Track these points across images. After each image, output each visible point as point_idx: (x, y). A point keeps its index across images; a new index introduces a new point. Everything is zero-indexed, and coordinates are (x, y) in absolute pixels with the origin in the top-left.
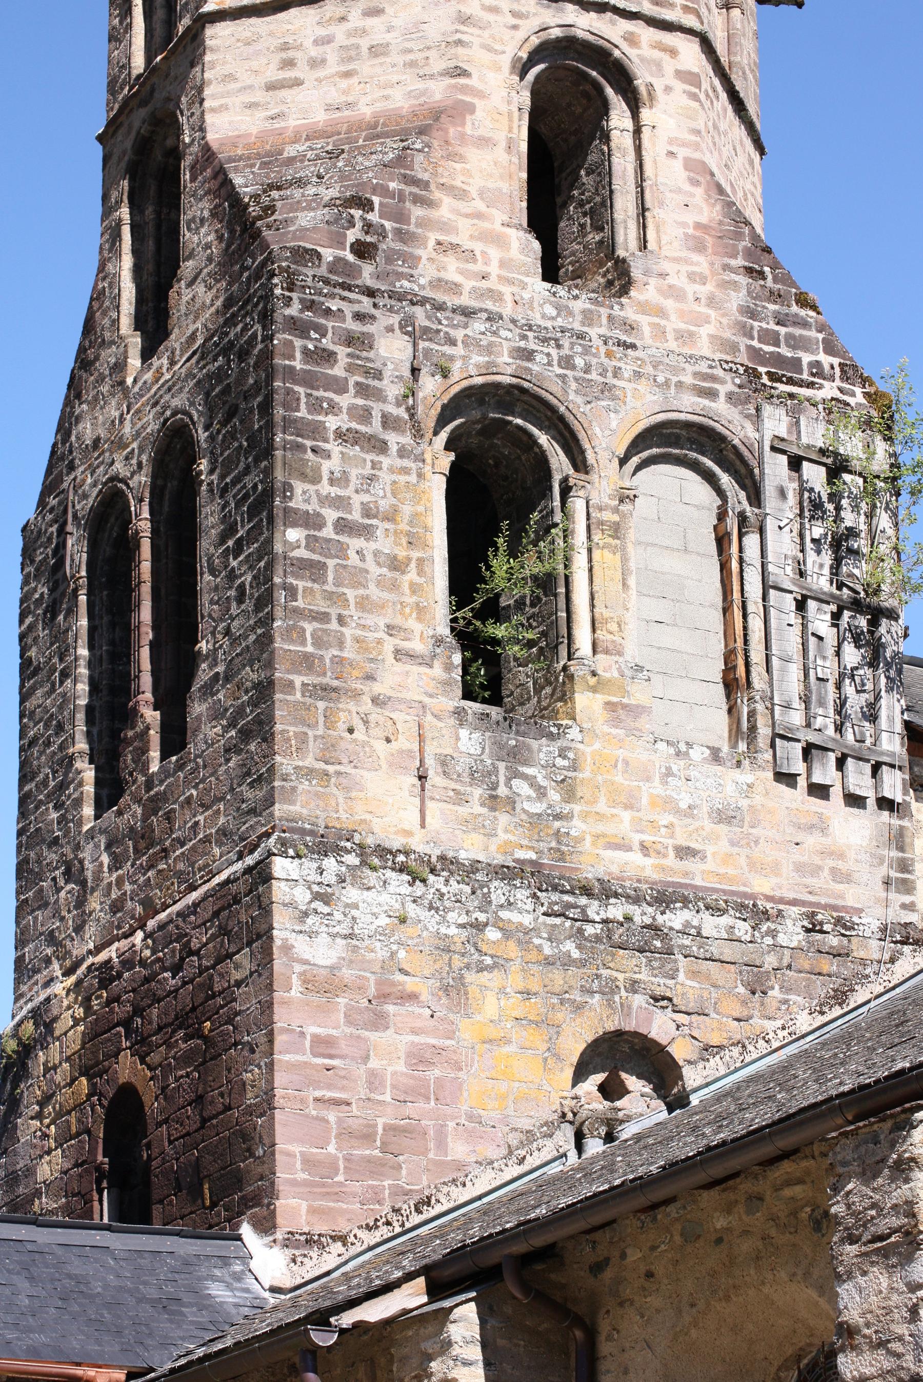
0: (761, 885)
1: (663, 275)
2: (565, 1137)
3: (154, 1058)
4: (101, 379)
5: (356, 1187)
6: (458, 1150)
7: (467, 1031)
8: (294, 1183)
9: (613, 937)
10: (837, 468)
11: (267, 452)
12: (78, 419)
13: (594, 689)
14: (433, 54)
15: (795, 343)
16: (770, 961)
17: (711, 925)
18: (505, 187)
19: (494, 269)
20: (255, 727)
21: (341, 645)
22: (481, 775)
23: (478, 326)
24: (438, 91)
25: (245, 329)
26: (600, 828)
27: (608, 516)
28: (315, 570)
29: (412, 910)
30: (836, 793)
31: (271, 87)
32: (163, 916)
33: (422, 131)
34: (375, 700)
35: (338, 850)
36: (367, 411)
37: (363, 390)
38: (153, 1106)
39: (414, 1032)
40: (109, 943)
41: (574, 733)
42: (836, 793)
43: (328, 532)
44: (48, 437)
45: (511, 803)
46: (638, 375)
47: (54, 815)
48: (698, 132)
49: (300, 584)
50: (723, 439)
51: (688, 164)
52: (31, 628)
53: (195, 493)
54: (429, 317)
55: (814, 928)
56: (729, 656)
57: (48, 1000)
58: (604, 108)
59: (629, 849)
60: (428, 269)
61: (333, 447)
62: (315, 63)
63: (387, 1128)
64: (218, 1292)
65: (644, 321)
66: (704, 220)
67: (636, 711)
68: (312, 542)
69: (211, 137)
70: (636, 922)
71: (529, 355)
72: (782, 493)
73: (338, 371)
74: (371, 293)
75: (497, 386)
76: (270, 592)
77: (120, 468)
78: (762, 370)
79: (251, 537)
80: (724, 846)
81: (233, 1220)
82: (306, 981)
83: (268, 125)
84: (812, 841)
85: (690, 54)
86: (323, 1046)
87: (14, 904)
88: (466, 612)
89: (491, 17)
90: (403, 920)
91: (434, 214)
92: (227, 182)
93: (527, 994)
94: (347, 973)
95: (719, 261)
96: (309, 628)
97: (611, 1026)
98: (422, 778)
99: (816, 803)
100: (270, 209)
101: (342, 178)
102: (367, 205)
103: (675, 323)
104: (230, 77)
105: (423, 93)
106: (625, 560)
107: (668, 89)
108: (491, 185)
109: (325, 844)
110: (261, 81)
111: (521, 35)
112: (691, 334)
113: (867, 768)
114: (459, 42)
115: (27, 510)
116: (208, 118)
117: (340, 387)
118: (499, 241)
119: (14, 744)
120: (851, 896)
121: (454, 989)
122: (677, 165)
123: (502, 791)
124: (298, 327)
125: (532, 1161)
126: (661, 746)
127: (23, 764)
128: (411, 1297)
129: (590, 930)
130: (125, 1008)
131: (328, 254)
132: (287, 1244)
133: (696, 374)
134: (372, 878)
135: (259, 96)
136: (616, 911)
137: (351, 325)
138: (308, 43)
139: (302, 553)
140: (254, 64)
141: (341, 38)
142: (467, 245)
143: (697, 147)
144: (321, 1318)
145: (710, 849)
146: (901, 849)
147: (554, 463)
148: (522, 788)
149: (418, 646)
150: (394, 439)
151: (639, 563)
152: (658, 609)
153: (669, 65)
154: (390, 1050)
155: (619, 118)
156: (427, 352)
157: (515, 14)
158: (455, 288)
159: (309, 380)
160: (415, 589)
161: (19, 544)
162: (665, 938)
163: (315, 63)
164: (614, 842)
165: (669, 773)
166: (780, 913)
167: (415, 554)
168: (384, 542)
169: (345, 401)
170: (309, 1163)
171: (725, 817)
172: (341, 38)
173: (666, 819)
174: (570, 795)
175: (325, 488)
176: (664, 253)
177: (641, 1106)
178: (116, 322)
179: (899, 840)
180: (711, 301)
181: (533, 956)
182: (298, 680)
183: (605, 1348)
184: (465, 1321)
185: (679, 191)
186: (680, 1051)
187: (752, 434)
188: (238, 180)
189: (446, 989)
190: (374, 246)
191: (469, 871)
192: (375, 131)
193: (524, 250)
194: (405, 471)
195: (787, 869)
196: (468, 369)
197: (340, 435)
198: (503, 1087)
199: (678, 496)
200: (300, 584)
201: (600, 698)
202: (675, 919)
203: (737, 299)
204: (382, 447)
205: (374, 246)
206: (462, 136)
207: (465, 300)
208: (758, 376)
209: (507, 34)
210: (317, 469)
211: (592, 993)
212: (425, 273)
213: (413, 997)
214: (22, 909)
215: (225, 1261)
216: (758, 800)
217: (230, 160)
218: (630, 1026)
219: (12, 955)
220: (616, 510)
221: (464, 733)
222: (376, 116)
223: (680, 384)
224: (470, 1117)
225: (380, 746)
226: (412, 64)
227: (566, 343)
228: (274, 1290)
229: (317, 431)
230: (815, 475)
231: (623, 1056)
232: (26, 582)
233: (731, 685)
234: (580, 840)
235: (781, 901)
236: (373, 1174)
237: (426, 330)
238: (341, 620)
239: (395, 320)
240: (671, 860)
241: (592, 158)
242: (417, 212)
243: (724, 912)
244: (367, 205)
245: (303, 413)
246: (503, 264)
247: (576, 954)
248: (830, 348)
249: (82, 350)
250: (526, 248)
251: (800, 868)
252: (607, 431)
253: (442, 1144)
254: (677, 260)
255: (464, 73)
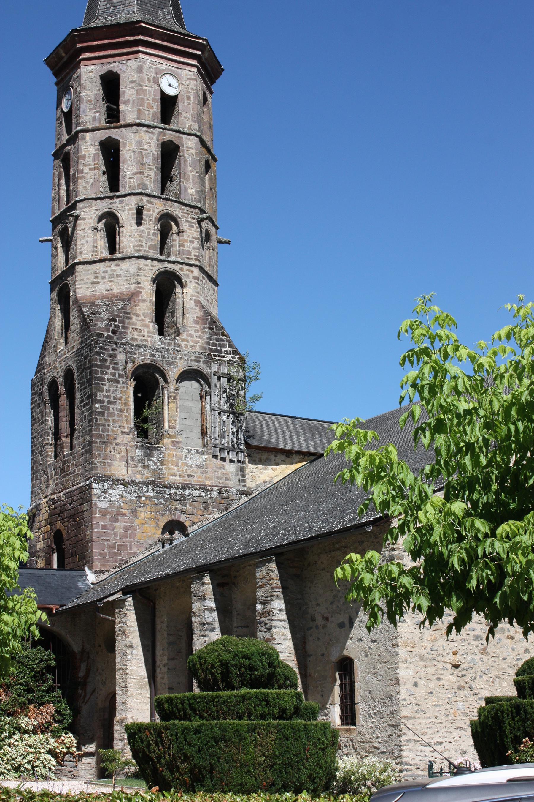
0: (208, 483)
1: (188, 331)
2: (159, 546)
3: (66, 524)
4: (50, 348)
5: (111, 559)
6: (135, 549)
7: (137, 522)
8: (97, 559)
9: (172, 497)
10: (230, 379)
11: (91, 385)
12: (45, 356)
13: (168, 438)
14: (132, 278)
15: (221, 345)
16: (210, 501)
17: (196, 493)
18: (149, 312)
19: (146, 334)
20: (88, 450)
21: (108, 431)
22: (142, 461)
23: (142, 349)
24: (133, 287)
25: (86, 352)
26: (170, 471)
27: (173, 395)
28: (102, 414)
29: (124, 494)
30: (227, 460)
31: (93, 283)
32: (67, 490)
33: (129, 300)
34: (116, 444)
35: (107, 481)
36: (115, 373)
37: (114, 368)
38: (64, 533)
39: (125, 522)
40: (54, 493)
41: (164, 449)
42: (227, 460)
43: (105, 404)
44: (37, 358)
45: (148, 467)
46: (181, 358)
47: (41, 458)
48: (198, 293)
49: (99, 417)
50: (202, 372)
51: (195, 301)
52: (34, 407)
53: (74, 389)
54: (129, 348)
55: (220, 492)
56: (202, 425)
57: (39, 504)
58: (175, 287)
59: (176, 476)
60: (131, 335)
61: (107, 383)
62: (103, 278)
63: (118, 545)
64: (80, 585)
65: (183, 344)
66: (198, 316)
67: (178, 442)
68: (101, 407)
69: (77, 295)
70: (177, 493)
71: (153, 356)
72: (216, 386)
73: (108, 364)
74: (116, 343)
75: (146, 364)
76: (92, 419)
77: (55, 374)
78: (212, 354)
79: (88, 404)
80: (199, 473)
81: (84, 566)
82: (100, 512)
83: (91, 293)
84: (221, 471)
85: (196, 272)
86: (104, 527)
87: (30, 477)
88: (138, 420)
89: (146, 268)
90: (122, 497)
91: (131, 321)
92: (81, 310)
93: (151, 512)
94: (109, 510)
95: (202, 326)
96: (101, 428)
97: (171, 519)
98: (127, 462)
99: (223, 463)
100: (92, 320)
101: (109, 313)
102: (115, 320)
103: (192, 340)
104: (82, 280)
105: (129, 288)
106: (177, 405)
107: (190, 282)
108: (146, 312)
109: (104, 479)
110: (89, 281)
111: (154, 271)
112: (195, 346)
113: (235, 453)
114: (138, 275)
115: (33, 376)
116: (77, 291)
117: (108, 367)
118: (147, 326)
119: (30, 437)
120: (230, 484)
121: (134, 512)
122: (192, 302)
123: (146, 464)
124: (98, 354)
125: (152, 551)
126: (185, 450)
127: (32, 443)
128: (119, 595)
129: (166, 496)
130: (58, 511)
131: (106, 334)
132: (95, 573)
133: (195, 357)
134: (115, 487)
135: (89, 285)
136: (173, 491)
137: (111, 352)
138: (101, 272)
139: (99, 410)
140: (88, 277)
141: (109, 272)
142: (140, 328)
143: (197, 296)
144: (100, 600)
145: (196, 475)
146: (243, 472)
147: (160, 381)
148: (151, 463)
149: (126, 430)
150: (121, 380)
151: (180, 407)
152: (184, 415)
153: (191, 275)
154: (119, 527)
155: (178, 290)
156: (129, 357)
157: (152, 266)
158: (136, 340)
159: (101, 367)
160: (126, 416)
161: (30, 385)
162: (184, 497)
163: (103, 278)
164: (173, 475)
165: (186, 457)
166: (212, 490)
167: (126, 408)
168: (118, 406)
169: (109, 371)
170: (100, 554)
171: (199, 467)
172: (109, 272)
173: (185, 468)
174: (162, 463)
175: (105, 393)
176: (189, 325)
177: (179, 538)
178: (54, 334)
179: (242, 470)
180: (200, 337)
181: (153, 503)
182: (98, 441)
183: (157, 607)
184: (130, 601)
185: (193, 309)
186: (187, 524)
187: (209, 371)
188: (84, 310)
189: (132, 512)
190: (117, 331)
191: (137, 484)
192: (118, 298)
193: (154, 328)
194: (124, 387)
195: (214, 478)
196: (139, 360)
197: (108, 380)
198: (145, 534)
199: (191, 387)
200: (99, 417)
201: (170, 440)
202: (187, 492)
203: (206, 335)
204: (118, 382)
205: (117, 331)
206: (139, 300)
207: (139, 342)
208: (211, 355)
209: (150, 272)
210: (103, 389)
211: (166, 511)
212: (129, 336)
213: (125, 514)
214: (32, 479)
215: (81, 576)
216: (208, 462)
217: (82, 303)
218: (176, 518)
219: (30, 490)
220: (175, 393)
221: (137, 450)
222: (118, 293)
223: (191, 360)
224: (138, 542)
225: (117, 455)
226: (127, 280)
227: (163, 352)
228: (92, 584)
229: (103, 379)
230: (224, 380)
231: (174, 526)
232: (32, 395)
233: (203, 433)
234: (164, 474)
235: (213, 486)
236: (115, 556)
237: (129, 352)
238: (108, 425)
239: (121, 350)
240: (186, 478)
241: (172, 298)
242: (128, 321)
243: (198, 490)
244: (115, 320)
245: (99, 375)
246: (148, 332)
247: (163, 502)
248: (230, 346)
249: (46, 338)
250: (153, 327)
251: (217, 478)
252: (173, 373)
253: (131, 549)
254: (191, 327)
255: (139, 283)
